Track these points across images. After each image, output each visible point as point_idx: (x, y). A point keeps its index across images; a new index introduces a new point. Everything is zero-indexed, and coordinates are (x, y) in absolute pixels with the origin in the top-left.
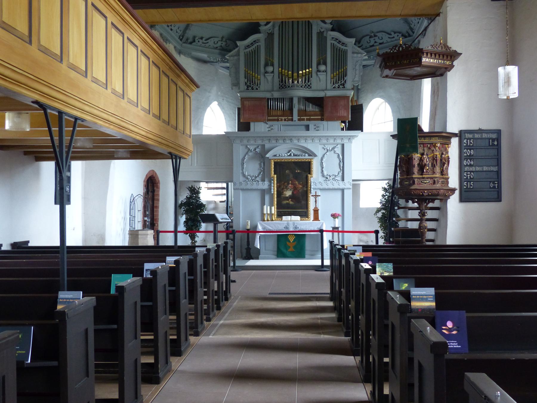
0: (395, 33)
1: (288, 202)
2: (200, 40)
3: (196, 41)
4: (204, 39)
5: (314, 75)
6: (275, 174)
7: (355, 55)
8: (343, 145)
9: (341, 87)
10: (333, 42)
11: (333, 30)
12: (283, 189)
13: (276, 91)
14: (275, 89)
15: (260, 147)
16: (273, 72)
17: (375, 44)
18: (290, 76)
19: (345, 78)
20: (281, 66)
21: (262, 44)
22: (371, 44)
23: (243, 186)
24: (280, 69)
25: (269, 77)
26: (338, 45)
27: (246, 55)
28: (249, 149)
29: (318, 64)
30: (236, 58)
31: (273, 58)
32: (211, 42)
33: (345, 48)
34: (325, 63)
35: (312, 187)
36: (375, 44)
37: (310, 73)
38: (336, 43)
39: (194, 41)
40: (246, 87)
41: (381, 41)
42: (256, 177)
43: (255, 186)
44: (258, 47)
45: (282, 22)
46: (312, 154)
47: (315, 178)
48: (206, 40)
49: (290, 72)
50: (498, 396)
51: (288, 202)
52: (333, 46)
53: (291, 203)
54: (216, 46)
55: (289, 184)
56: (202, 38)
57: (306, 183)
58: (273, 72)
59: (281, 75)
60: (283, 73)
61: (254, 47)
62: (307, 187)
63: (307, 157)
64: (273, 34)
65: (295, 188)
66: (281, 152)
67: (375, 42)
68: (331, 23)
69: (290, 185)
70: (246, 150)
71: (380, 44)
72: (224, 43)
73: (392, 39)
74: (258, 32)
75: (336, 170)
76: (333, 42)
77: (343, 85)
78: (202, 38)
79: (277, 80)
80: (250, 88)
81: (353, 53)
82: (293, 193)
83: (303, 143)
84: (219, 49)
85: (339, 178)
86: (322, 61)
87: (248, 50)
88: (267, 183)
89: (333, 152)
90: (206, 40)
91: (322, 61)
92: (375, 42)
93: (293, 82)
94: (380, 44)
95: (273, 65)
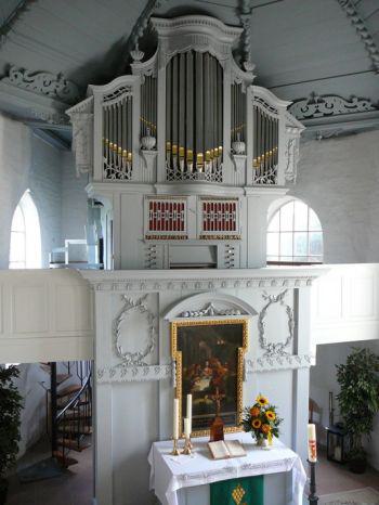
0: (360, 100)
1: (202, 400)
2: (19, 74)
3: (12, 75)
4: (26, 74)
5: (226, 157)
6: (179, 349)
7: (289, 130)
8: (296, 292)
9: (269, 181)
10: (257, 104)
11: (256, 83)
12: (194, 377)
13: (163, 183)
14: (159, 179)
15: (149, 298)
16: (155, 148)
17: (315, 115)
18: (182, 154)
19: (276, 167)
20: (170, 138)
21: (136, 95)
22: (307, 114)
23: (117, 377)
24: (169, 143)
25: (149, 156)
26: (264, 109)
27: (107, 113)
28: (128, 303)
29: (234, 140)
30: (85, 116)
31: (156, 123)
32: (38, 81)
33: (274, 116)
34: (244, 140)
35: (247, 370)
36: (315, 115)
37: (221, 154)
38: (261, 106)
39: (7, 74)
40: (106, 173)
41: (329, 111)
42: (141, 357)
43: (140, 376)
44: (129, 102)
45: (178, 55)
46: (247, 310)
47: (251, 353)
48: (30, 76)
49: (182, 149)
50: (204, 351)
51: (202, 400)
52: (257, 110)
53: (209, 402)
54: (45, 89)
55: (204, 366)
56: (22, 71)
57: (234, 362)
58: (155, 148)
59: (169, 150)
60: (175, 152)
61: (120, 99)
62: (237, 372)
63: (237, 318)
64: (156, 79)
65: (216, 374)
66: (191, 311)
67: (317, 112)
68: (254, 72)
69: (206, 369)
70: (123, 304)
71: (325, 115)
72: (62, 86)
73: (351, 110)
74: (128, 71)
75: (285, 334)
76: (257, 104)
77: (272, 178)
78: (22, 71)
79: (162, 164)
80: (114, 176)
81: (288, 126)
82: (211, 383)
83: (231, 291)
84: (53, 98)
85: (289, 349)
86: (239, 136)
87: (106, 104)
88: (163, 369)
89: (279, 302)
90: (30, 76)
91: (239, 136)
92: (317, 112)
93: (195, 169)
94: (325, 115)
95: (155, 135)
